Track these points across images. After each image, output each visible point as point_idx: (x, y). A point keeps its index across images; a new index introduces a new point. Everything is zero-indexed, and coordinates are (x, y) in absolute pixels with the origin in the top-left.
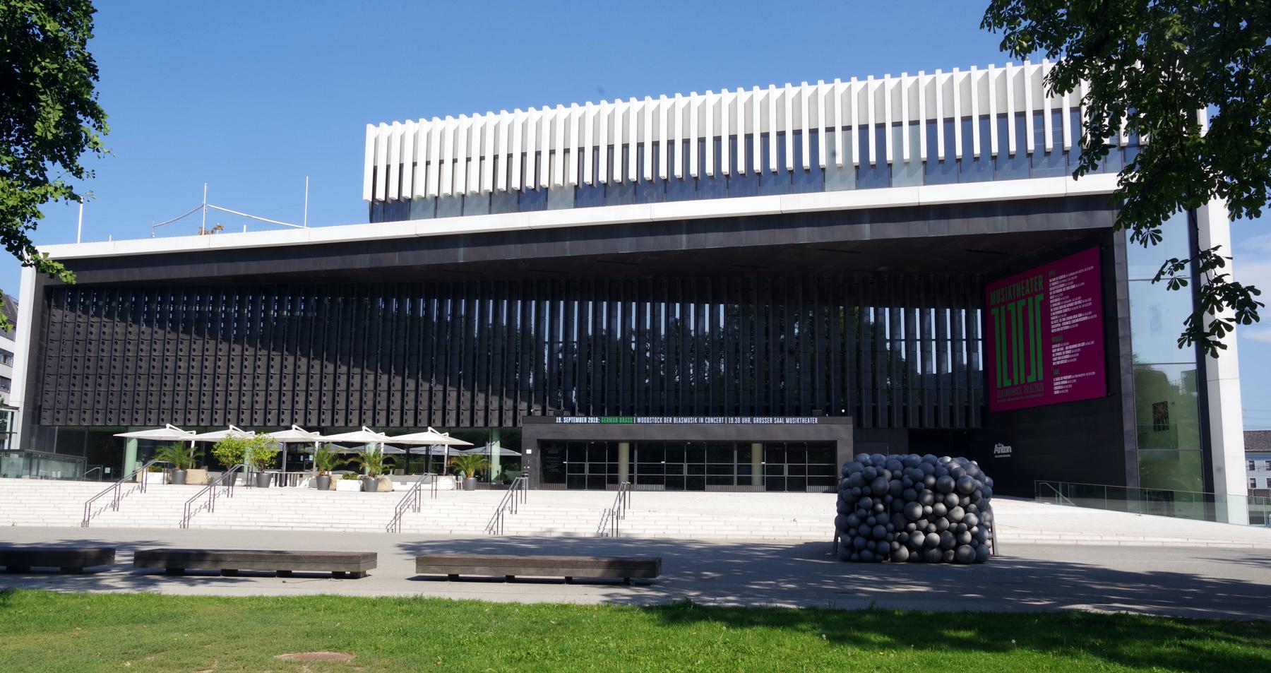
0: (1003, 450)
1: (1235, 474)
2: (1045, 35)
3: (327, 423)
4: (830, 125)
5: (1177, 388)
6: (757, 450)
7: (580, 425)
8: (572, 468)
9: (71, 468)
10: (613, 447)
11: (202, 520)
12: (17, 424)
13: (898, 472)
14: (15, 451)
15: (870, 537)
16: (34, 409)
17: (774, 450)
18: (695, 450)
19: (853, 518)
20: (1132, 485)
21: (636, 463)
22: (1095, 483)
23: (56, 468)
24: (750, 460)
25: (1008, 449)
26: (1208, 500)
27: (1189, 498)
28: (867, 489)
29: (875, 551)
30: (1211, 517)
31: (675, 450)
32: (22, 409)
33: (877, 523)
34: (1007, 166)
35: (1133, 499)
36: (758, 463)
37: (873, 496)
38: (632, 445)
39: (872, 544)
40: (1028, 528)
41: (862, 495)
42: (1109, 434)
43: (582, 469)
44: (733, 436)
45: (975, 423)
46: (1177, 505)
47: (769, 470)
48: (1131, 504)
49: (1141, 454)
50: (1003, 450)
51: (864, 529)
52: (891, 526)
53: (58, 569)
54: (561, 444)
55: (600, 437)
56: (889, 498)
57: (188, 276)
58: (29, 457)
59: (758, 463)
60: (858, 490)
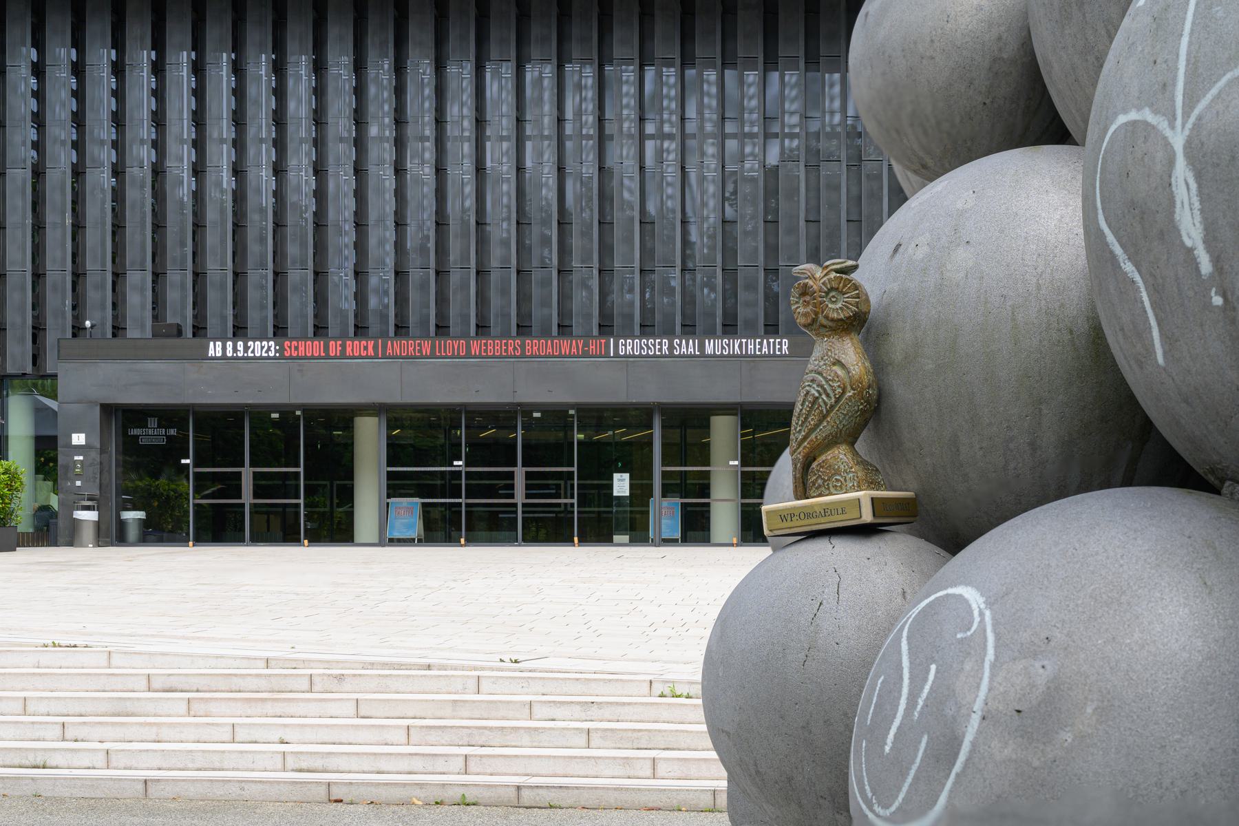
7: (243, 367)
36: (725, 470)
44: (650, 392)
54: (170, 415)
59: (725, 470)
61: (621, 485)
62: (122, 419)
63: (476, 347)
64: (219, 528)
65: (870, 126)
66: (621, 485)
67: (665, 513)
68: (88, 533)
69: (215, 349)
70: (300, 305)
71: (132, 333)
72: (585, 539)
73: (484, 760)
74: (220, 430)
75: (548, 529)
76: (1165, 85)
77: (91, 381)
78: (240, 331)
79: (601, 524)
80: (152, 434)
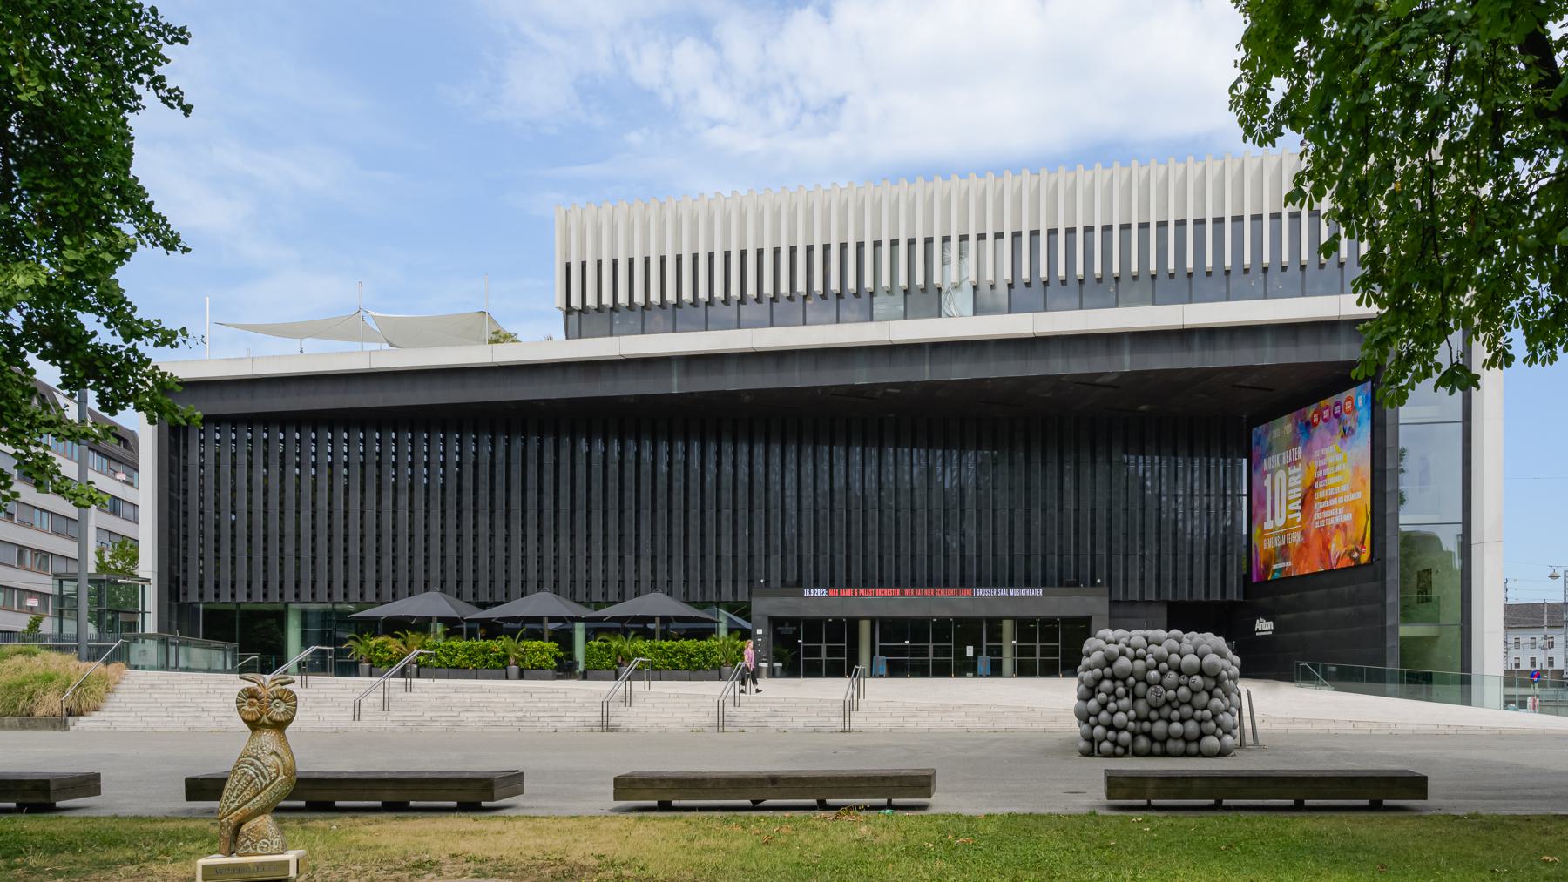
0: (1264, 626)
1: (1492, 651)
2: (1564, 104)
3: (483, 597)
4: (1257, 222)
5: (1450, 554)
6: (1007, 626)
7: (817, 600)
8: (808, 652)
9: (217, 658)
10: (854, 623)
11: (373, 719)
12: (150, 599)
13: (1141, 651)
14: (150, 636)
15: (1110, 727)
16: (171, 581)
17: (1025, 628)
18: (942, 628)
19: (1093, 703)
20: (1393, 665)
21: (878, 644)
22: (1357, 667)
23: (198, 654)
24: (1000, 640)
25: (1270, 625)
26: (1462, 685)
27: (1444, 681)
28: (1107, 671)
29: (1115, 743)
30: (1466, 700)
31: (919, 628)
32: (154, 581)
33: (1118, 710)
34: (658, 317)
35: (1393, 681)
36: (1009, 643)
37: (1113, 678)
38: (873, 620)
39: (1111, 734)
40: (1292, 717)
41: (1103, 678)
42: (1374, 612)
43: (817, 652)
44: (982, 612)
45: (1234, 595)
46: (1436, 688)
47: (1020, 651)
48: (1390, 687)
49: (1405, 631)
50: (1264, 626)
51: (1104, 716)
52: (1132, 713)
53: (302, 803)
54: (794, 621)
55: (838, 613)
56: (1132, 680)
57: (381, 404)
58: (164, 642)
59: (1009, 643)
60: (1097, 671)
61: (970, 651)
62: (775, 622)
63: (927, 592)
64: (921, 671)
65: (1338, 438)
66: (970, 651)
67: (984, 662)
68: (764, 673)
69: (807, 593)
70: (841, 572)
71: (772, 584)
72: (956, 675)
73: (205, 666)
74: (813, 627)
75: (942, 671)
76: (51, 679)
77: (765, 606)
78: (816, 585)
79: (966, 668)
80: (788, 630)
